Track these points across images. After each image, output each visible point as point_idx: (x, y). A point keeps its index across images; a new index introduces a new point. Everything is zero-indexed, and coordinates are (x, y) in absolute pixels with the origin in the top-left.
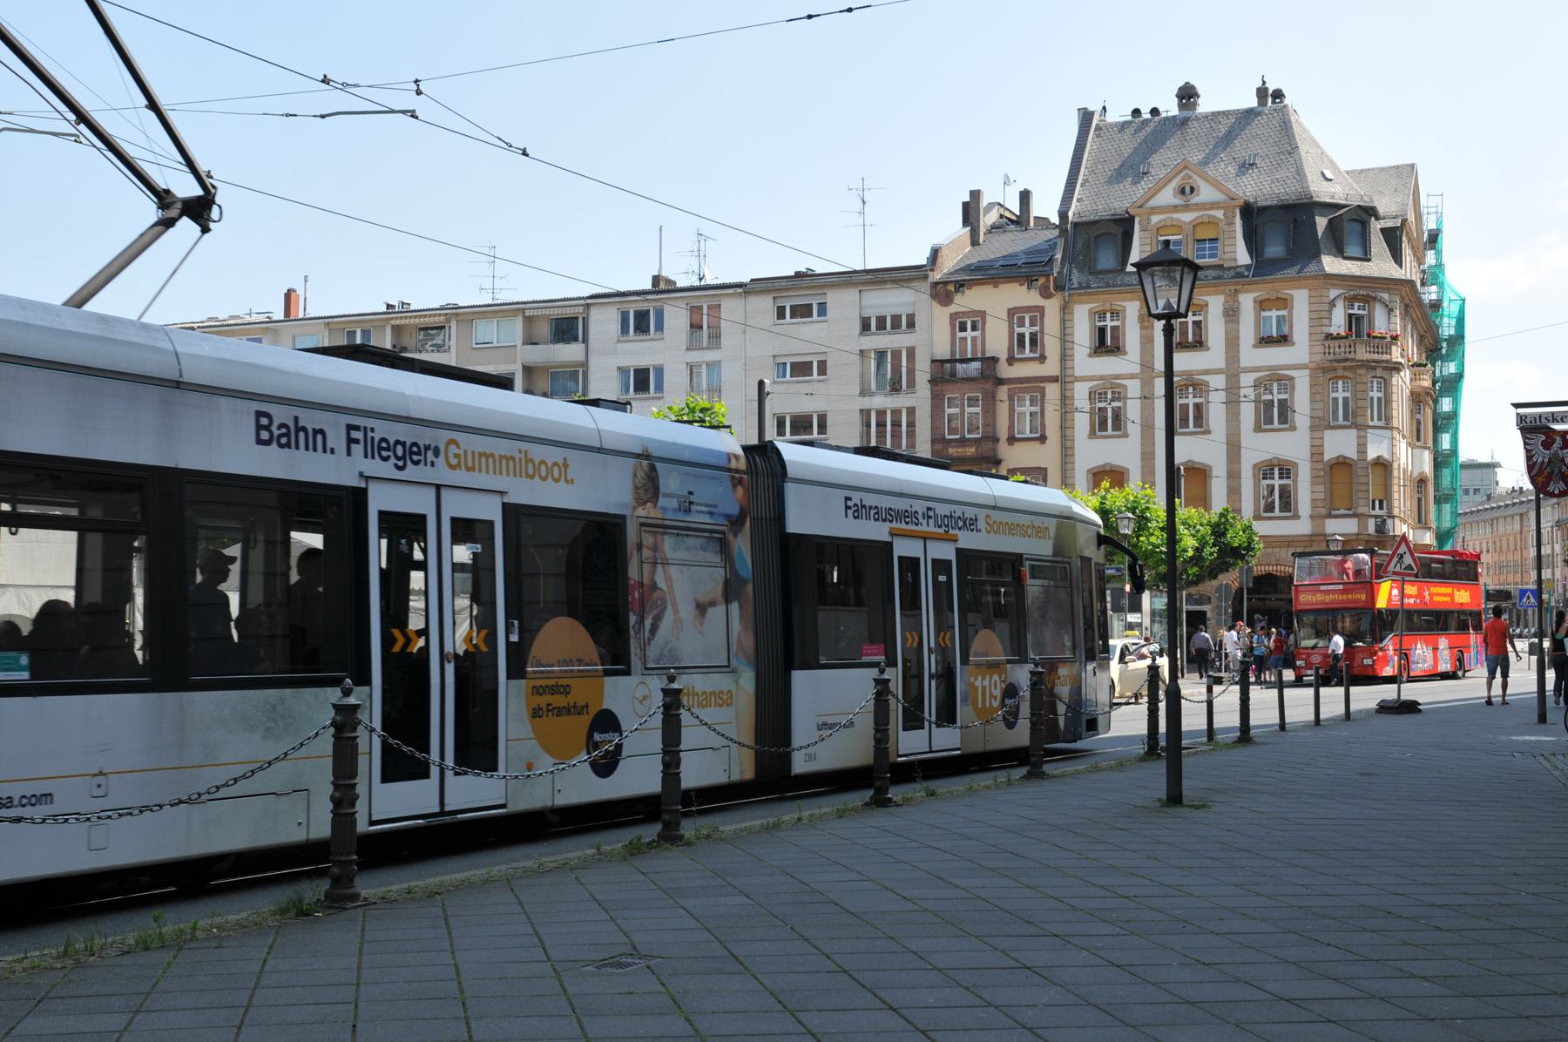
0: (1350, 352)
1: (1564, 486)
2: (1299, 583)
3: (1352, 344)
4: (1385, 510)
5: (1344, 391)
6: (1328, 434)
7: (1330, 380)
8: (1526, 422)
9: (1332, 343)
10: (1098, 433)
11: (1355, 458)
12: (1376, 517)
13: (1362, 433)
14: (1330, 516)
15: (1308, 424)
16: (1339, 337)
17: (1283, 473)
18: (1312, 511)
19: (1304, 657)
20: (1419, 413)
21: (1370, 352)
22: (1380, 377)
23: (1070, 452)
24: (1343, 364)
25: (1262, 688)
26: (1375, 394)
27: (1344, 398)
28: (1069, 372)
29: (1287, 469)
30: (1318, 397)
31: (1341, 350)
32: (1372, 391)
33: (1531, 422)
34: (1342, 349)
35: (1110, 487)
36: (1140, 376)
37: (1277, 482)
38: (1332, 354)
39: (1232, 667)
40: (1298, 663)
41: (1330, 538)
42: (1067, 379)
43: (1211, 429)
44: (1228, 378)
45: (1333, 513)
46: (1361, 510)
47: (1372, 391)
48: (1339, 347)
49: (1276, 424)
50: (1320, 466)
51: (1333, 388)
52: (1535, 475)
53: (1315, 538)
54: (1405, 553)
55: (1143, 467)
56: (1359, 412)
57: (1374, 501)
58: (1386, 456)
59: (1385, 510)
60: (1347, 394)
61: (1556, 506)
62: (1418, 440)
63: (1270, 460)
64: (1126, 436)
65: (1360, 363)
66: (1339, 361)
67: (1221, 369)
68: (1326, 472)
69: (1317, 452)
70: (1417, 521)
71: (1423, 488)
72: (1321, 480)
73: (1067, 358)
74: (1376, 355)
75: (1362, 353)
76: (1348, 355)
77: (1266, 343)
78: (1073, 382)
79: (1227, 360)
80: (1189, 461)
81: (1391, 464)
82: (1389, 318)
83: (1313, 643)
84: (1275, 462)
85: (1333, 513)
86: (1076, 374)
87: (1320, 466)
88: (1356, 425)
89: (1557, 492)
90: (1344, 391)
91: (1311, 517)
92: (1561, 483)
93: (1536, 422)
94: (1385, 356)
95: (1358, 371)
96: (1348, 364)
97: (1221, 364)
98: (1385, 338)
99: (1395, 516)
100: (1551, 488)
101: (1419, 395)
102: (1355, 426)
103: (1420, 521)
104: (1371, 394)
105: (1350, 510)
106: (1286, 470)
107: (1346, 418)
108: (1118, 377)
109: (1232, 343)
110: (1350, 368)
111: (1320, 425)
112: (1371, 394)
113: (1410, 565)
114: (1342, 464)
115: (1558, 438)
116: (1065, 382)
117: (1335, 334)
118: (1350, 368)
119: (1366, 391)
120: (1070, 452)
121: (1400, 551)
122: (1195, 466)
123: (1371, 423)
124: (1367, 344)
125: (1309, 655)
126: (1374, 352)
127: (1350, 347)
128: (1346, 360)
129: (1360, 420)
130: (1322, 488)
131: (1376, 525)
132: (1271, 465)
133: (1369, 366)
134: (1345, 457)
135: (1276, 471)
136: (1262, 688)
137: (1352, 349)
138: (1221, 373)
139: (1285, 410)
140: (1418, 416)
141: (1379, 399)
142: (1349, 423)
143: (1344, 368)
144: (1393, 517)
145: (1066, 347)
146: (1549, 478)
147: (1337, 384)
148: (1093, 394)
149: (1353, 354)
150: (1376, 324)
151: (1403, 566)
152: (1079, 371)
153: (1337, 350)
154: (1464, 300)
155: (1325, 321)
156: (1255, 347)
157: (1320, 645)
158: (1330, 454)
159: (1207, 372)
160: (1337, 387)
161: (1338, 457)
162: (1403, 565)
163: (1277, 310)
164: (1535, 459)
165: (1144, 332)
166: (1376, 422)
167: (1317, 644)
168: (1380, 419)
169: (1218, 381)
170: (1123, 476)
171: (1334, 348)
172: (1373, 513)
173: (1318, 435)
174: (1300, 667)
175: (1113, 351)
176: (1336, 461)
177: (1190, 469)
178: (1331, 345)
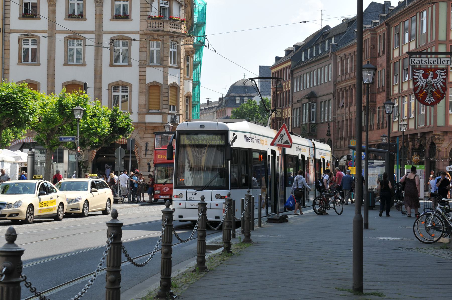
0: (161, 27)
1: (433, 100)
2: (157, 149)
3: (162, 23)
4: (175, 111)
5: (157, 47)
6: (148, 70)
7: (150, 41)
8: (414, 63)
9: (152, 21)
10: (23, 62)
11: (162, 83)
12: (171, 114)
13: (166, 70)
14: (148, 113)
15: (139, 64)
16: (155, 18)
17: (126, 89)
18: (139, 110)
19: (159, 188)
20: (188, 61)
21: (171, 27)
22: (175, 41)
23: (7, 72)
24: (157, 33)
25: (139, 206)
26: (173, 50)
27: (157, 51)
28: (7, 27)
29: (126, 87)
30: (144, 50)
31: (155, 25)
32: (171, 48)
33: (417, 63)
34: (157, 25)
35: (66, 92)
36: (48, 32)
37: (120, 94)
38: (151, 27)
39: (122, 194)
40: (156, 192)
41: (166, 125)
42: (6, 31)
43: (86, 63)
44: (96, 36)
45: (150, 111)
46: (164, 110)
47: (171, 48)
48: (156, 24)
49: (121, 63)
50: (143, 86)
51: (151, 45)
52: (418, 93)
53: (139, 124)
54: (284, 134)
55: (48, 82)
56: (165, 59)
57: (170, 106)
58: (177, 83)
59: (175, 111)
60: (159, 49)
61: (215, 113)
62: (188, 76)
63: (118, 82)
64: (39, 64)
65: (166, 33)
66: (155, 31)
67: (93, 31)
68: (146, 90)
69: (142, 79)
70: (185, 118)
71: (189, 100)
72: (144, 94)
73: (6, 19)
74: (174, 29)
75: (167, 28)
76: (160, 28)
77: (117, 18)
78: (9, 33)
79: (95, 29)
80: (74, 80)
81: (179, 87)
82: (180, 10)
83: (164, 182)
84: (120, 83)
85: (150, 111)
86: (12, 28)
87: (143, 86)
88: (163, 65)
89: (429, 103)
90: (157, 47)
91: (138, 113)
92: (432, 98)
93: (419, 63)
94: (178, 30)
95: (165, 37)
96: (160, 33)
97: (93, 28)
98: (178, 20)
99: (180, 114)
100: (426, 101)
101: (188, 52)
102: (162, 66)
103: (187, 118)
104: (171, 50)
105: (158, 110)
106: (126, 87)
107: (157, 61)
108: (35, 31)
109: (99, 17)
110: (161, 35)
111: (143, 65)
112: (171, 50)
113: (287, 141)
114: (155, 86)
115: (431, 73)
116: (5, 33)
117: (153, 16)
118: (161, 35)
119: (168, 48)
120: (7, 72)
121: (282, 133)
122: (77, 83)
123: (170, 65)
124: (170, 23)
125: (162, 188)
126: (173, 28)
127: (161, 24)
128: (159, 31)
129: (165, 63)
130: (144, 98)
131: (171, 119)
132: (118, 85)
133: (171, 35)
134: (157, 82)
135: (120, 88)
136: (139, 206)
137: (162, 25)
138: (92, 33)
139: (127, 57)
140: (188, 63)
141: (174, 52)
142: (159, 64)
143: (158, 35)
144: (180, 115)
145: (6, 13)
146: (426, 95)
147: (154, 43)
148: (20, 40)
149: (162, 27)
150: (173, 13)
151: (283, 142)
152: (12, 27)
153: (154, 25)
154: (206, 4)
155: (148, 9)
156: (111, 20)
157: (168, 182)
158: (149, 80)
159: (85, 32)
160: (154, 45)
161: (153, 82)
162: (283, 141)
163: (123, 1)
164: (418, 84)
165: (51, 7)
166: (172, 65)
167: (166, 181)
168: (174, 63)
169: (90, 39)
170: (37, 87)
171: (153, 24)
172: (170, 112)
173: (143, 69)
174: (157, 194)
175: (33, 17)
176: (152, 84)
177: (74, 84)
178: (151, 22)
